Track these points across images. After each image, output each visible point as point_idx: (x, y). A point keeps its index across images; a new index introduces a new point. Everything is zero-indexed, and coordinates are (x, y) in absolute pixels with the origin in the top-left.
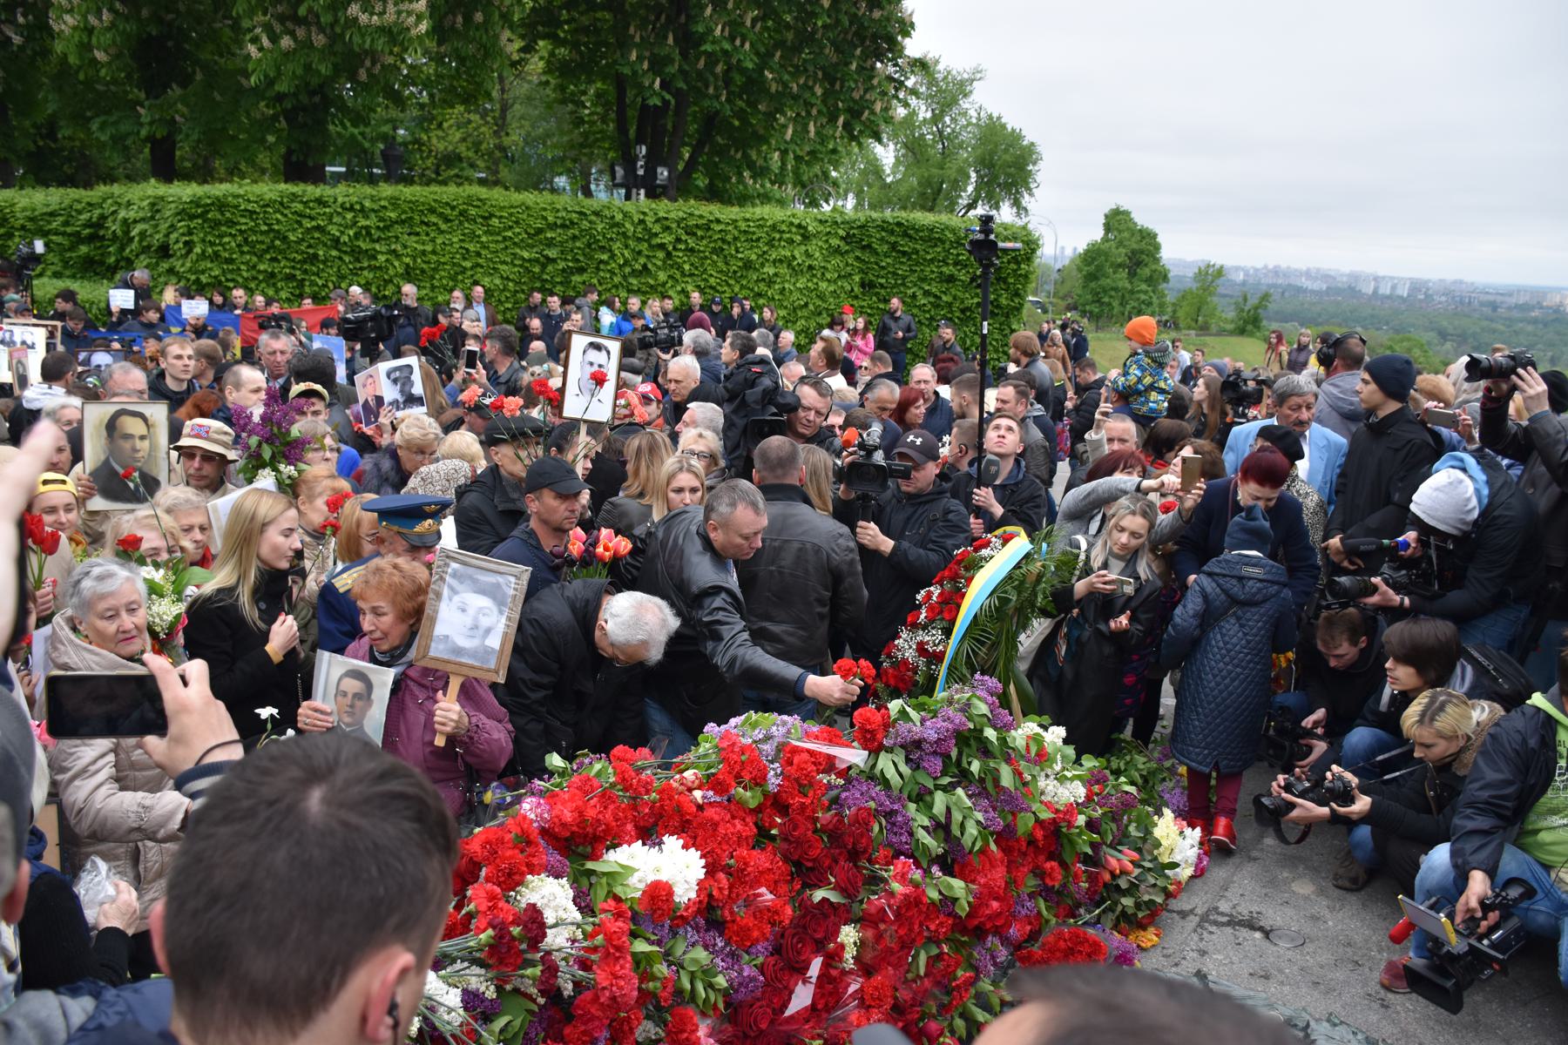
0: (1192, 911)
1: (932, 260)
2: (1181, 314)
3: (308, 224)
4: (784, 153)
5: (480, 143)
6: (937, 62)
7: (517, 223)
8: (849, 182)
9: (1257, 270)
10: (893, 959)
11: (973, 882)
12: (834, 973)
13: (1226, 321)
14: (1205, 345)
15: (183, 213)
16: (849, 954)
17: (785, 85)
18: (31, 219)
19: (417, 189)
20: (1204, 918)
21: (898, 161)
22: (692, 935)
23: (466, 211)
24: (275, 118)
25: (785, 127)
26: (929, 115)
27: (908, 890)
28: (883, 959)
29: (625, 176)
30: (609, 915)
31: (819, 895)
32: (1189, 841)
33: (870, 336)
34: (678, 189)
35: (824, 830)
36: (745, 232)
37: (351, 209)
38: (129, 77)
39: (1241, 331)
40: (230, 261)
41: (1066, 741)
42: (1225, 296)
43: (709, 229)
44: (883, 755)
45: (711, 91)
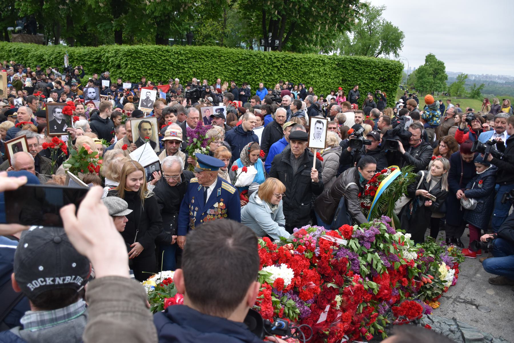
0: (451, 297)
1: (367, 72)
2: (451, 91)
3: (163, 58)
4: (317, 35)
5: (217, 31)
6: (370, 4)
7: (230, 58)
8: (338, 45)
9: (479, 76)
10: (352, 307)
11: (379, 283)
12: (333, 310)
13: (467, 94)
14: (460, 102)
15: (125, 55)
16: (338, 305)
17: (318, 12)
18: (79, 56)
19: (198, 47)
20: (455, 300)
21: (355, 38)
22: (289, 296)
23: (213, 54)
24: (153, 24)
25: (318, 26)
26: (366, 22)
27: (358, 285)
28: (349, 307)
29: (265, 43)
30: (265, 288)
31: (329, 285)
32: (450, 274)
33: (345, 97)
34: (282, 47)
35: (332, 264)
36: (304, 62)
37: (177, 53)
38: (109, 11)
39: (473, 97)
40: (139, 70)
41: (411, 239)
42: (467, 85)
43: (292, 61)
44: (351, 240)
45: (294, 15)
